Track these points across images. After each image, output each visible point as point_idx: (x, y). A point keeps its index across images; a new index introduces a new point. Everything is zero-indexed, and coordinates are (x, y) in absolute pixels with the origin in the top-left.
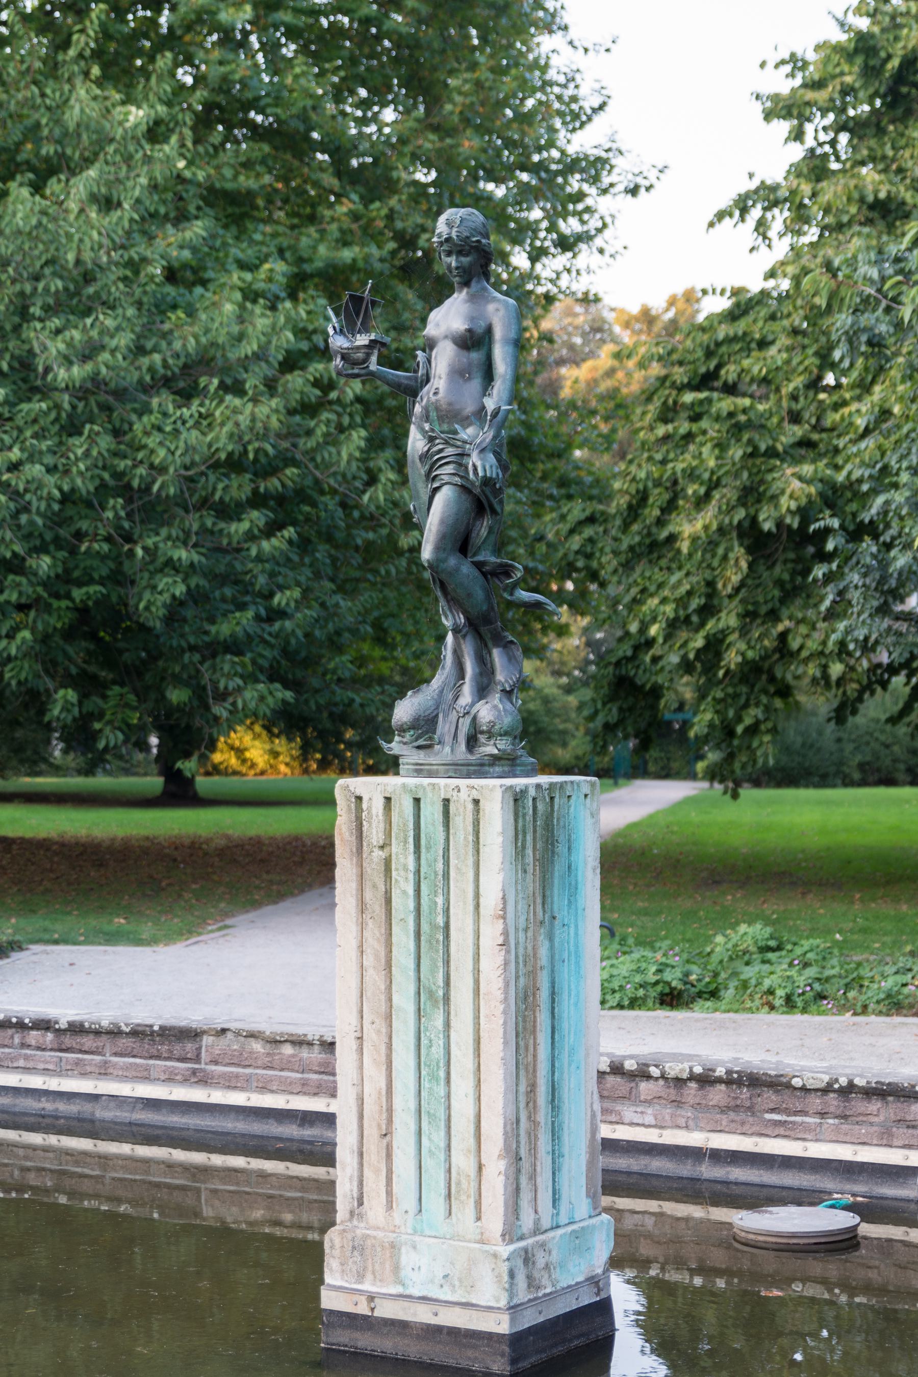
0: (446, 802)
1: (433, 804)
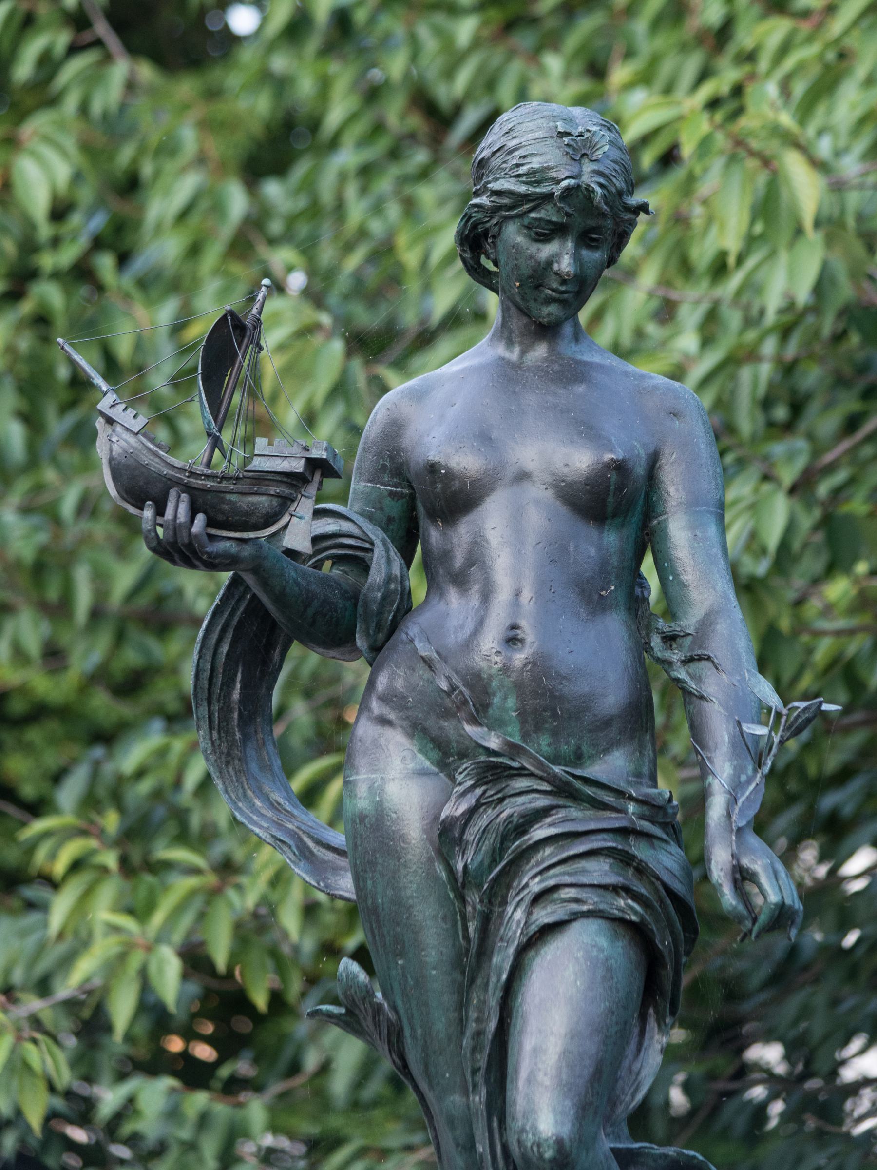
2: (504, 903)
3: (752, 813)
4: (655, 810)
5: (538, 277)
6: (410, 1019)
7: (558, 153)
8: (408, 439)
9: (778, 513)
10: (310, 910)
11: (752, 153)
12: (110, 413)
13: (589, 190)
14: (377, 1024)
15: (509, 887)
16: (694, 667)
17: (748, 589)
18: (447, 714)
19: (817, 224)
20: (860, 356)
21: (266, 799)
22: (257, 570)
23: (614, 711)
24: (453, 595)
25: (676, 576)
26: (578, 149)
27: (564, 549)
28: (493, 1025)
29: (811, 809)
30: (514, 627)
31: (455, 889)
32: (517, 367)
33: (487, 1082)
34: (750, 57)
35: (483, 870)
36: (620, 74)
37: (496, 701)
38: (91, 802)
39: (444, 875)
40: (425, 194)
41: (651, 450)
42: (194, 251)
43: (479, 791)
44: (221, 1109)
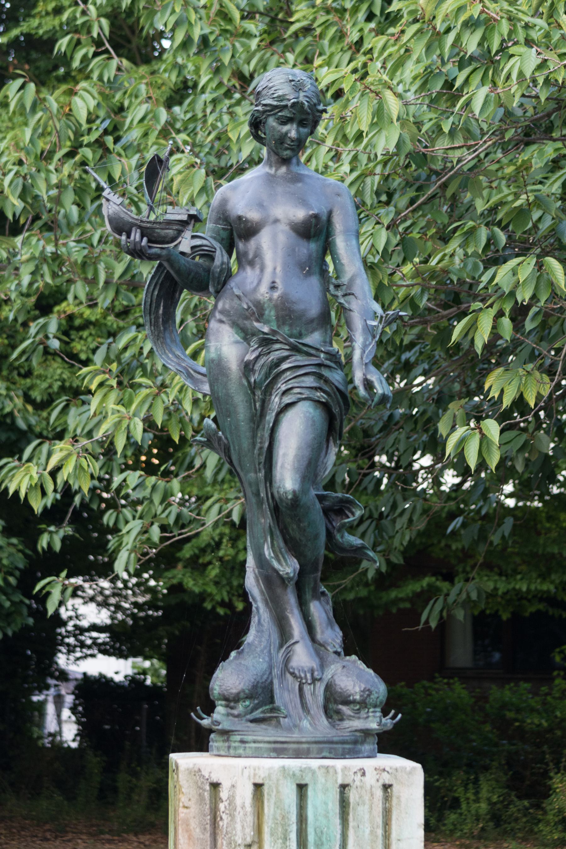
0: (344, 787)
1: (326, 790)
2: (271, 395)
3: (371, 357)
4: (333, 356)
5: (282, 139)
6: (233, 443)
7: (290, 88)
8: (230, 206)
9: (383, 237)
10: (196, 402)
11: (372, 91)
12: (108, 197)
13: (303, 104)
14: (219, 445)
15: (272, 388)
16: (347, 298)
17: (370, 268)
18: (247, 318)
19: (398, 119)
20: (415, 174)
21: (174, 354)
22: (169, 260)
23: (315, 316)
24: (248, 269)
25: (340, 261)
26: (298, 87)
27: (294, 250)
28: (266, 445)
29: (399, 359)
30: (274, 282)
31: (251, 389)
32: (274, 176)
33: (265, 468)
34: (370, 51)
35: (261, 382)
36: (317, 62)
37: (267, 312)
38: (108, 360)
39: (246, 384)
40: (239, 110)
41: (329, 209)
42: (146, 135)
43: (260, 349)
44: (161, 483)
